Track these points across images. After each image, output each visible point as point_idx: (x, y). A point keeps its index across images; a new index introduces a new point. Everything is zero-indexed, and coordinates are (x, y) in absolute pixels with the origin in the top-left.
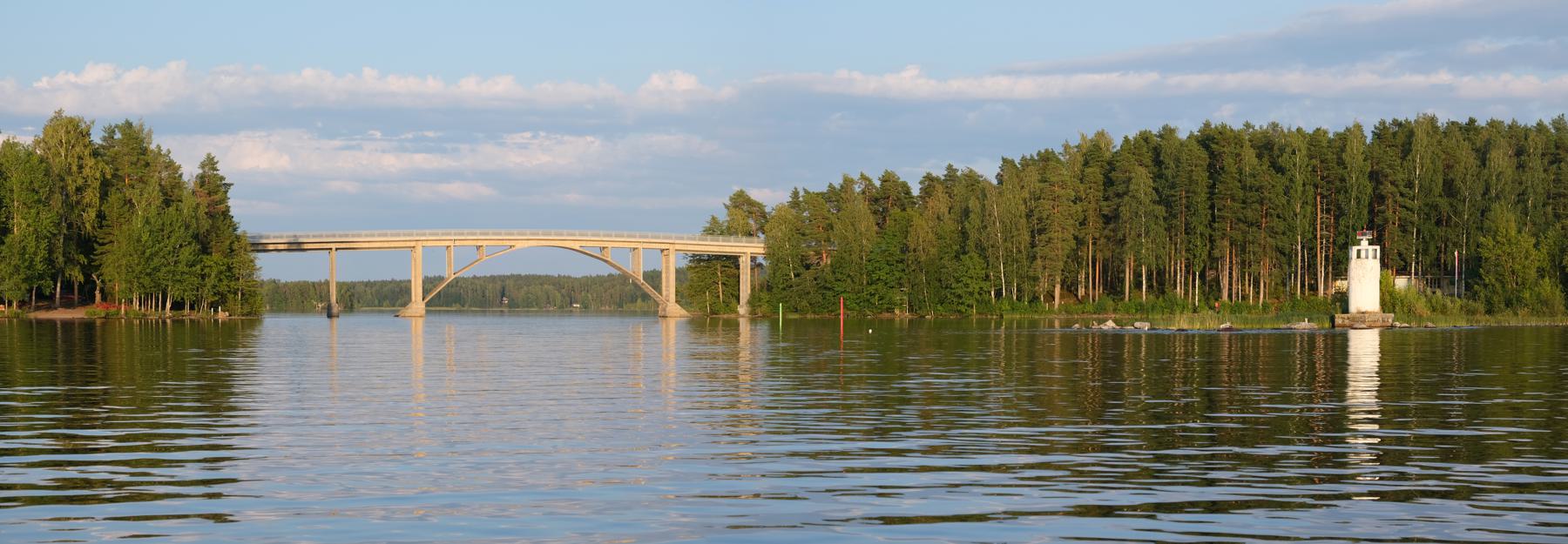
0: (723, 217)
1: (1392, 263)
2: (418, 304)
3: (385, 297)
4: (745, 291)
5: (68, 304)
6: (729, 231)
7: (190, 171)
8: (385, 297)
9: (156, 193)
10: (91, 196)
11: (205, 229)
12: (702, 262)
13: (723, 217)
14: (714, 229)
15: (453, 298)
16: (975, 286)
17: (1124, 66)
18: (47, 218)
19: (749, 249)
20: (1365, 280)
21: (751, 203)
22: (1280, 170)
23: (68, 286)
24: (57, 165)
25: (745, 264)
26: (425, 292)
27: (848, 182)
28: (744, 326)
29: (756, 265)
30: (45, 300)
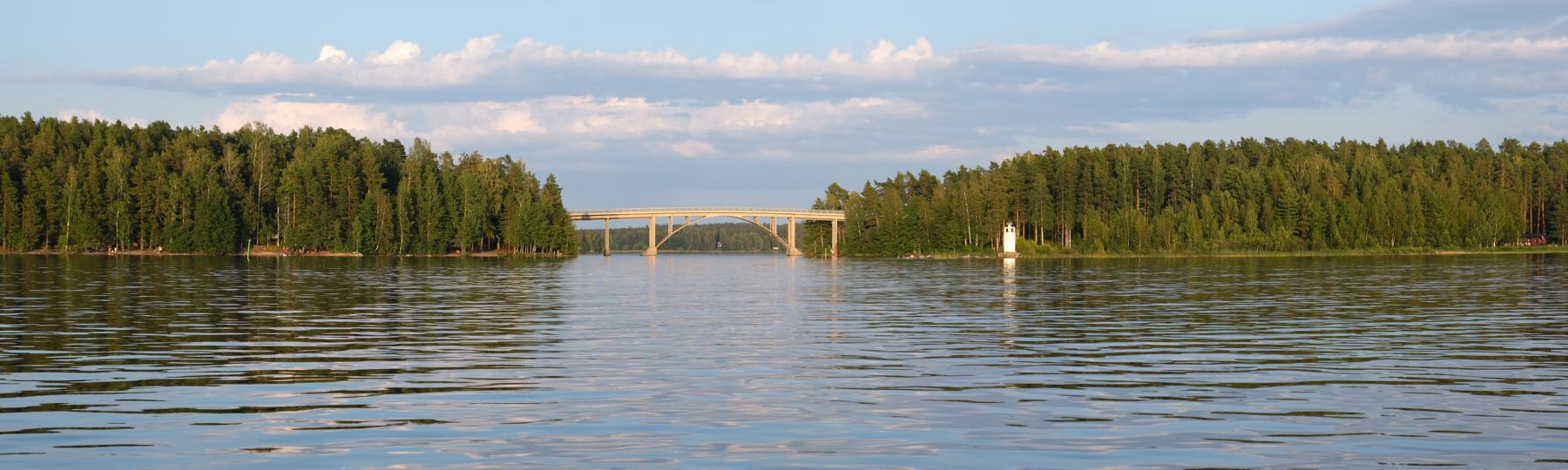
0: (824, 198)
1: (1027, 232)
2: (653, 249)
3: (624, 242)
4: (834, 241)
5: (486, 250)
6: (828, 207)
7: (542, 184)
8: (624, 242)
9: (528, 195)
10: (498, 197)
11: (556, 215)
12: (810, 223)
13: (824, 198)
14: (818, 206)
15: (681, 241)
16: (953, 238)
17: (1317, 34)
18: (481, 209)
19: (836, 217)
20: (1010, 239)
21: (840, 190)
22: (1115, 175)
23: (486, 242)
24: (485, 182)
25: (835, 224)
26: (658, 239)
27: (900, 177)
28: (834, 258)
29: (840, 223)
30: (477, 248)
